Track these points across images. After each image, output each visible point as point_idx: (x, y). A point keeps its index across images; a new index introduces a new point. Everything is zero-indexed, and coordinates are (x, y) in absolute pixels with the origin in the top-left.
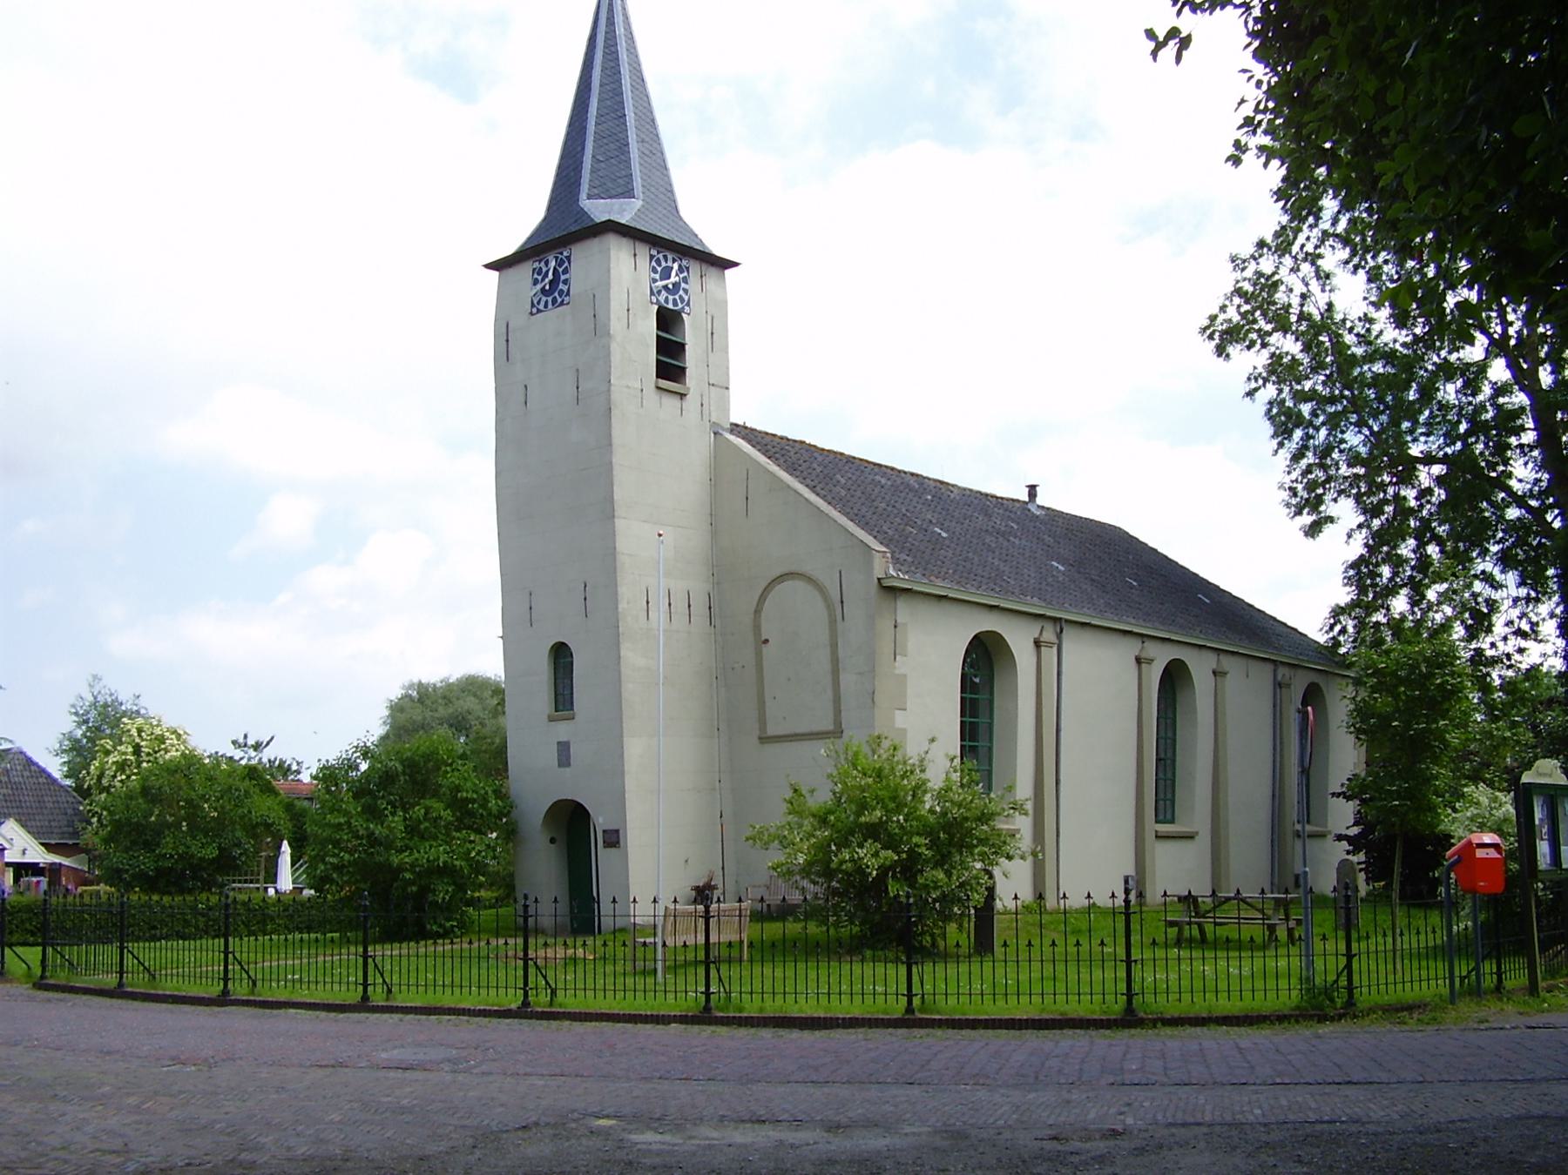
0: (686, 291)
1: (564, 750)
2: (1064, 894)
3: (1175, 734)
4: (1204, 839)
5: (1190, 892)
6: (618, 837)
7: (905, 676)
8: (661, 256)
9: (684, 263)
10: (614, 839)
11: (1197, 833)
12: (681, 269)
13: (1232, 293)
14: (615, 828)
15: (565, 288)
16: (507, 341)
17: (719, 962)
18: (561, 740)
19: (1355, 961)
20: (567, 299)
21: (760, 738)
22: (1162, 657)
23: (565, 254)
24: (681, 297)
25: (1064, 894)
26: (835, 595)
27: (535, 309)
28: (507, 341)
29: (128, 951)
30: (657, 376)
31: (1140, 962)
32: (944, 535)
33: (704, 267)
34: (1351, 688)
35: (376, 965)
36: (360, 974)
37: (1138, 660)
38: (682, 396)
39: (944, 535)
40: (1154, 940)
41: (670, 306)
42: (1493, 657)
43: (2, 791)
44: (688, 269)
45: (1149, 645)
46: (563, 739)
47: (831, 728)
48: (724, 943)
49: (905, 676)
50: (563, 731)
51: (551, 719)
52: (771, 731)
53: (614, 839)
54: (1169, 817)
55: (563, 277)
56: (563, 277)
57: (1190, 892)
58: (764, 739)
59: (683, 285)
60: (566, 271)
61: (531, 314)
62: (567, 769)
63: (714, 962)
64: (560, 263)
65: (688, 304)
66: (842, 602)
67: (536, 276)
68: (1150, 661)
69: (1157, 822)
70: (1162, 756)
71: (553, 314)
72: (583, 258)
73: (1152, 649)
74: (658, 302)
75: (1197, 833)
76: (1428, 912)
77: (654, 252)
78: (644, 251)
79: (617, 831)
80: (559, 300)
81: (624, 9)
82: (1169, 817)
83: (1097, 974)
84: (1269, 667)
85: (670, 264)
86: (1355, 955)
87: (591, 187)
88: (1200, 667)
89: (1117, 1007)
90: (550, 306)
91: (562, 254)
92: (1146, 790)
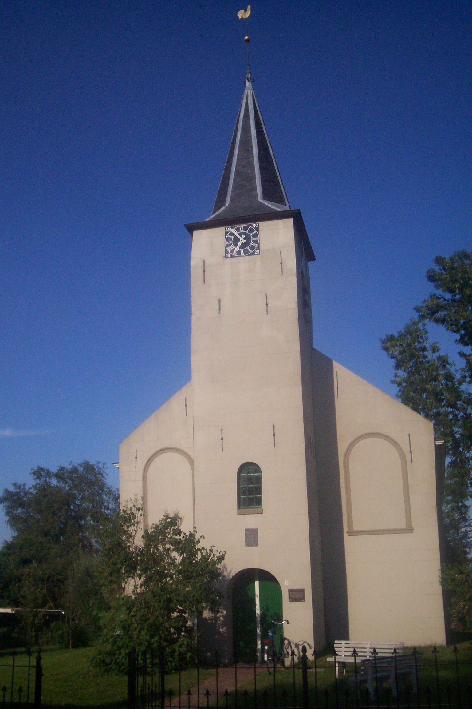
6: (304, 595)
13: (397, 377)
14: (302, 588)
15: (256, 245)
16: (204, 271)
18: (249, 527)
20: (257, 252)
26: (406, 448)
28: (204, 271)
42: (173, 577)
43: (471, 270)
46: (251, 526)
47: (404, 526)
60: (255, 235)
61: (225, 257)
62: (254, 548)
66: (411, 452)
89: (181, 706)
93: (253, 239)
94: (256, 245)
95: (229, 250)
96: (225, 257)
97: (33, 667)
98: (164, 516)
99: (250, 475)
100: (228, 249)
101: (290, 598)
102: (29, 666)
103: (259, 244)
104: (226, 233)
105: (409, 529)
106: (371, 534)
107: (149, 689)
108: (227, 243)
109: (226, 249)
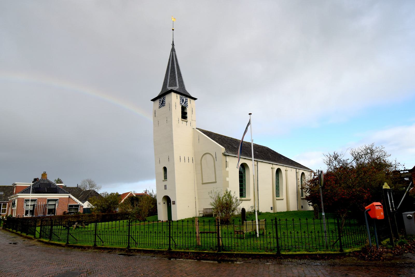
0: (187, 103)
1: (165, 186)
3: (279, 181)
4: (285, 200)
7: (228, 171)
8: (182, 97)
9: (187, 98)
10: (174, 203)
11: (284, 199)
12: (186, 99)
15: (164, 103)
17: (222, 237)
22: (276, 167)
24: (186, 104)
27: (160, 107)
29: (132, 237)
30: (182, 118)
32: (236, 147)
33: (191, 99)
34: (286, 242)
35: (173, 240)
36: (128, 233)
37: (272, 168)
38: (187, 122)
39: (236, 147)
41: (184, 106)
44: (187, 99)
45: (274, 165)
47: (215, 181)
49: (228, 171)
50: (165, 183)
51: (163, 181)
54: (278, 196)
55: (164, 101)
56: (164, 101)
58: (203, 184)
59: (186, 102)
60: (165, 100)
61: (159, 108)
63: (221, 238)
64: (163, 98)
65: (187, 106)
68: (274, 168)
69: (276, 197)
70: (277, 185)
71: (163, 108)
72: (167, 98)
73: (274, 166)
74: (182, 105)
75: (284, 199)
77: (181, 96)
78: (179, 96)
79: (175, 201)
80: (164, 105)
81: (175, 54)
82: (278, 196)
84: (295, 169)
85: (184, 98)
87: (169, 85)
88: (283, 169)
90: (162, 106)
92: (274, 189)
105: (216, 182)
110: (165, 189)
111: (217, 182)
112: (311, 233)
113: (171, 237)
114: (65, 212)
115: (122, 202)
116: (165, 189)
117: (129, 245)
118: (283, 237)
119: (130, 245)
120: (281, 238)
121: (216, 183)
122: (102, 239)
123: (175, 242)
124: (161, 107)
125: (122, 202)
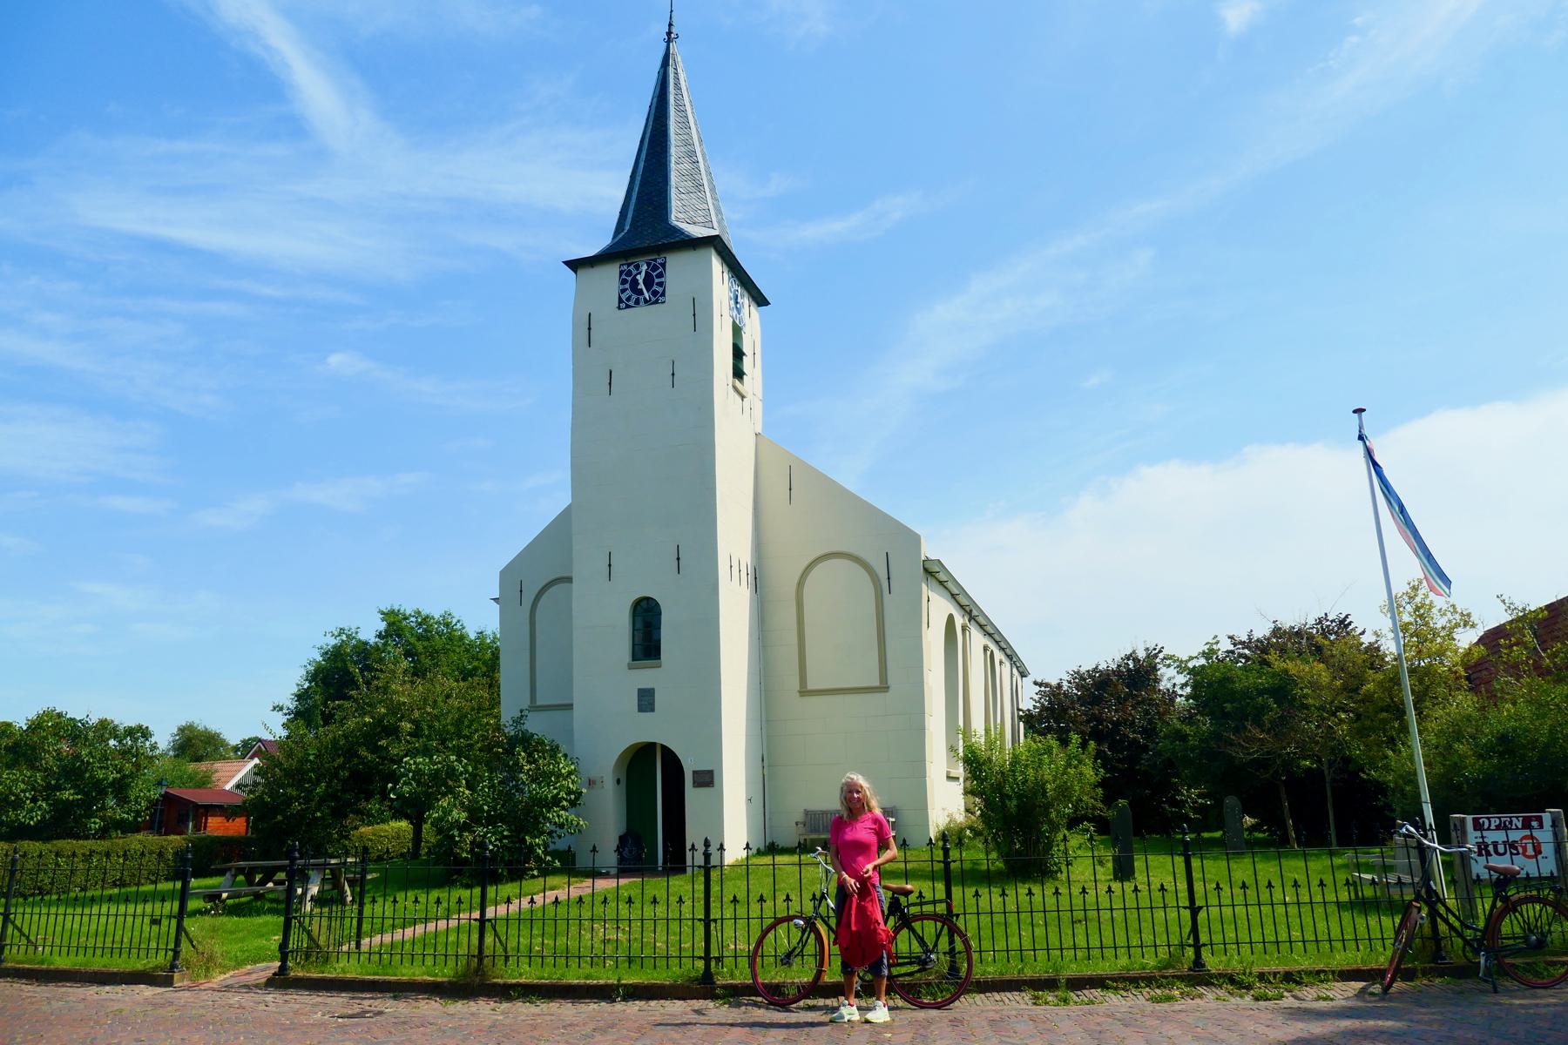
2: (693, 846)
5: (570, 847)
15: (660, 290)
19: (1202, 915)
21: (800, 692)
23: (659, 261)
25: (693, 846)
31: (719, 922)
40: (735, 897)
47: (877, 683)
48: (88, 897)
50: (646, 677)
51: (630, 667)
52: (811, 686)
53: (707, 779)
57: (570, 847)
60: (660, 275)
67: (624, 277)
76: (499, 887)
83: (573, 944)
86: (1200, 908)
91: (655, 260)
93: (657, 280)
94: (660, 290)
95: (624, 297)
96: (619, 308)
97: (700, 958)
98: (1478, 876)
99: (1562, 827)
100: (622, 296)
101: (694, 783)
102: (693, 957)
103: (620, 277)
104: (621, 273)
105: (883, 688)
106: (1556, 858)
107: (395, 901)
108: (622, 287)
109: (620, 298)
110: (641, 709)
111: (891, 690)
112: (1267, 887)
113: (489, 920)
114: (145, 733)
115: (191, 824)
116: (641, 709)
117: (707, 966)
118: (1213, 901)
119: (713, 969)
120: (722, 919)
121: (887, 694)
122: (316, 937)
123: (496, 935)
124: (631, 303)
125: (191, 824)
